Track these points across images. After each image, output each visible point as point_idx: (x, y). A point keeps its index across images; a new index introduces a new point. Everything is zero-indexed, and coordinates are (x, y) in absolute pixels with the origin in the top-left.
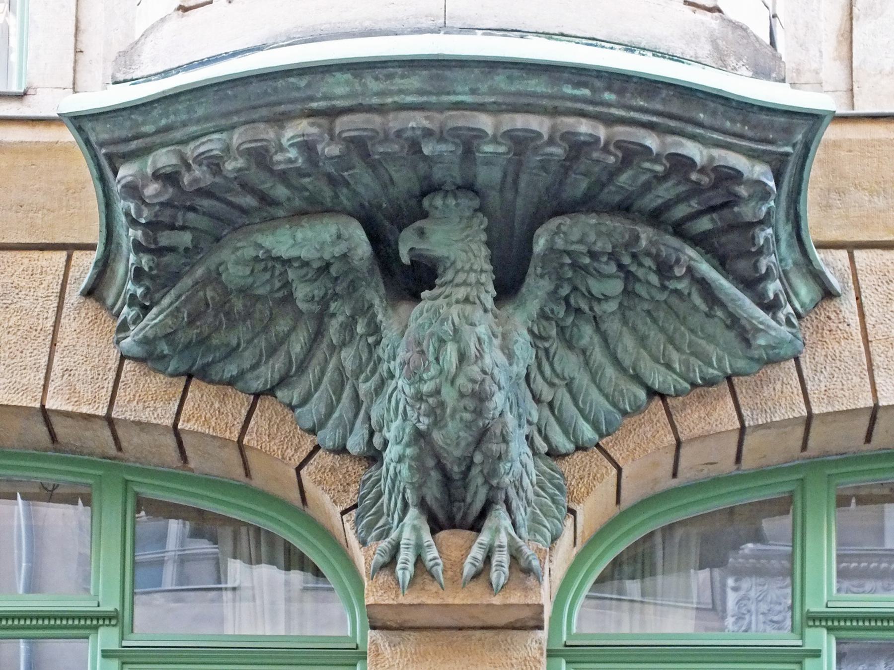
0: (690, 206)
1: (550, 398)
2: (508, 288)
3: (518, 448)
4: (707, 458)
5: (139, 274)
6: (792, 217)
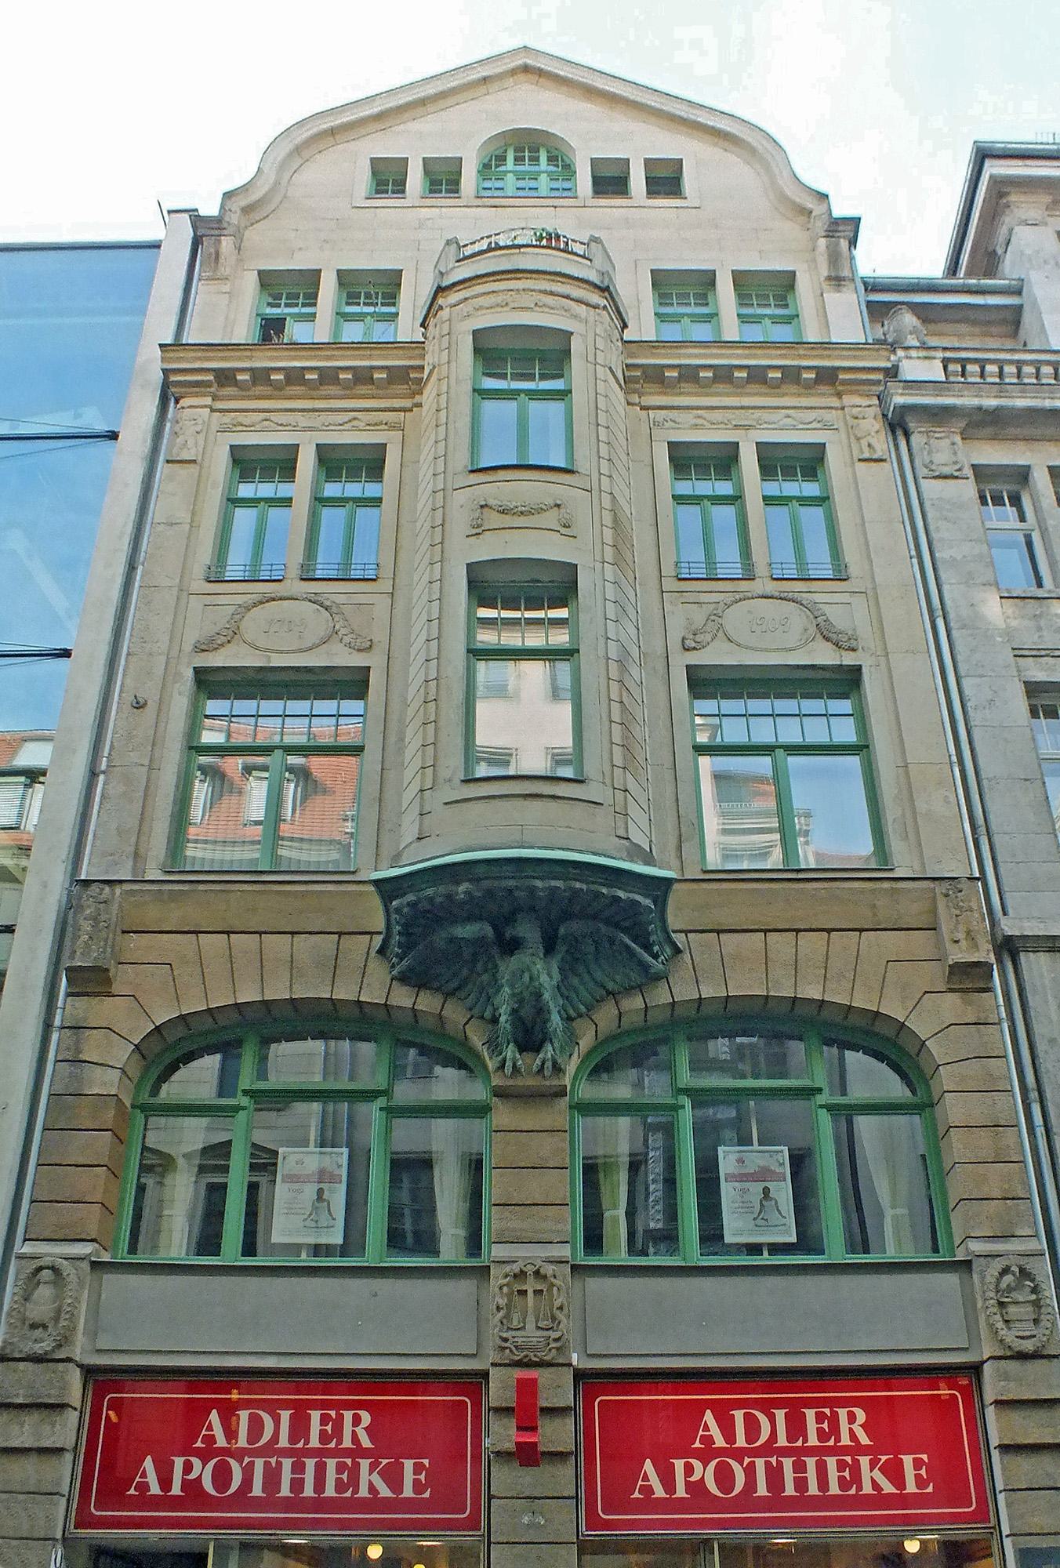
2: (549, 949)
4: (633, 1020)
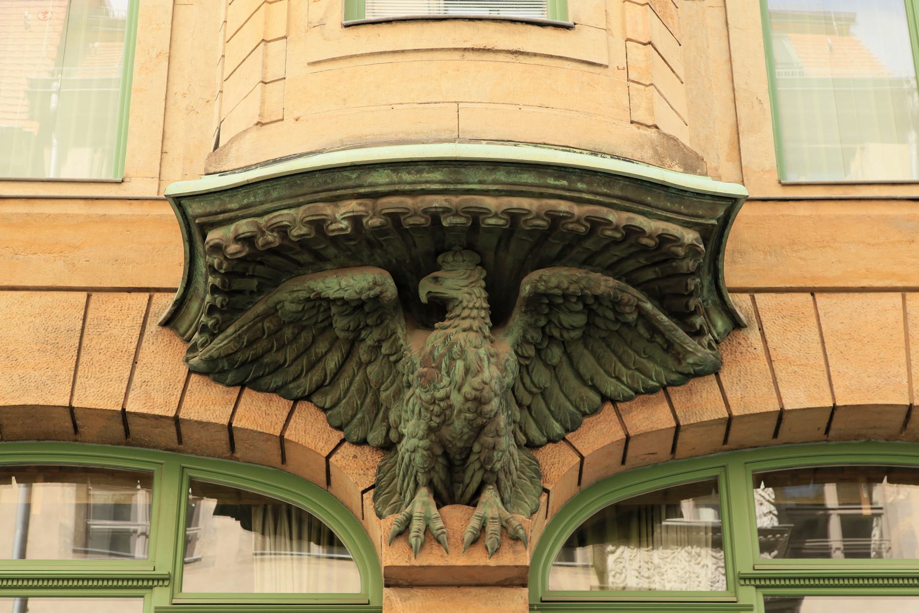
0: (639, 262)
1: (529, 403)
3: (506, 442)
5: (212, 309)
6: (712, 269)
